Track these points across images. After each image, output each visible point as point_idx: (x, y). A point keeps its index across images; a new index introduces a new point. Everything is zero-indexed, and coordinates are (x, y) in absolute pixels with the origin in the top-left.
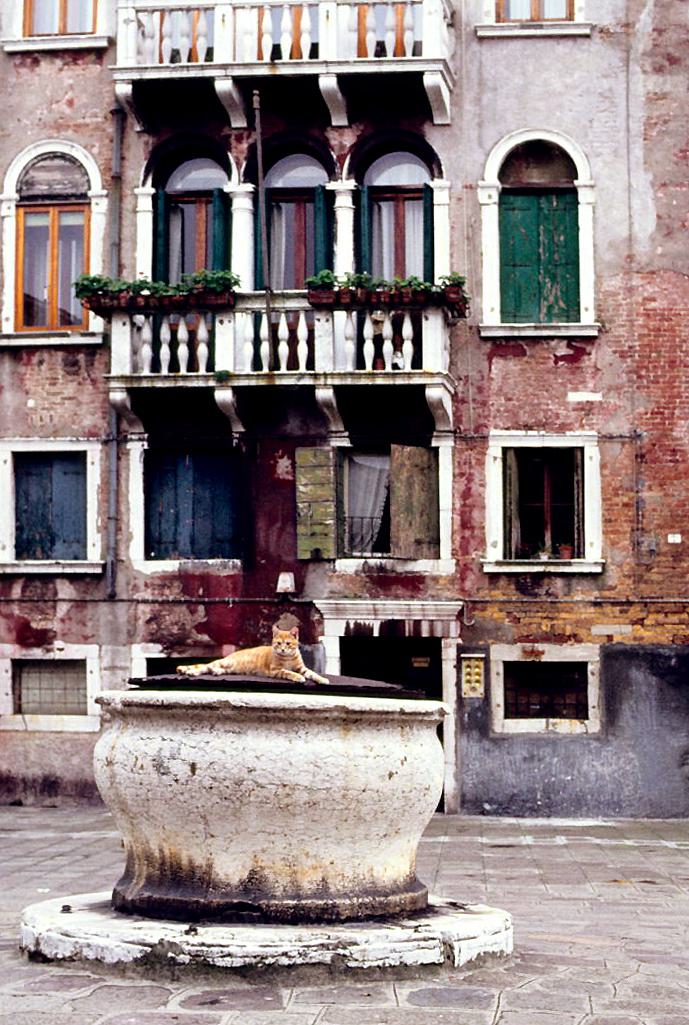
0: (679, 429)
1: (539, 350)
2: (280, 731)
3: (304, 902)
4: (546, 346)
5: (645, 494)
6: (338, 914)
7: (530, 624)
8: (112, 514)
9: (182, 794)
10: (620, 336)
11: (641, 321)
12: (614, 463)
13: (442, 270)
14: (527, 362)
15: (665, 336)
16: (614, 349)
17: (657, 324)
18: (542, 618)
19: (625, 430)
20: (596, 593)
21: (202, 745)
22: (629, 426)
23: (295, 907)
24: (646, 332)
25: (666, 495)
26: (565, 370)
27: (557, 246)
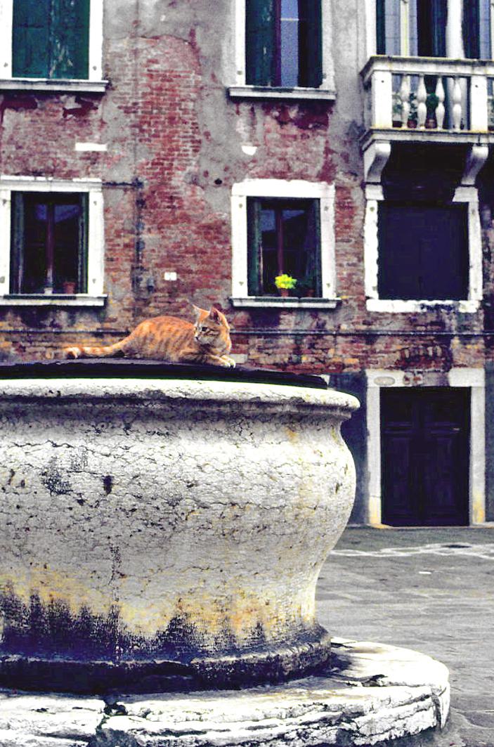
0: (176, 179)
1: (48, 104)
2: (219, 432)
3: (244, 657)
4: (56, 100)
5: (145, 237)
6: (282, 669)
7: (36, 352)
9: (88, 519)
10: (125, 93)
11: (145, 80)
12: (117, 208)
14: (37, 114)
15: (166, 94)
16: (119, 104)
17: (159, 83)
18: (46, 347)
19: (128, 178)
20: (98, 325)
21: (120, 452)
22: (133, 175)
23: (237, 665)
24: (149, 90)
25: (164, 237)
26: (74, 122)
27: (68, 11)
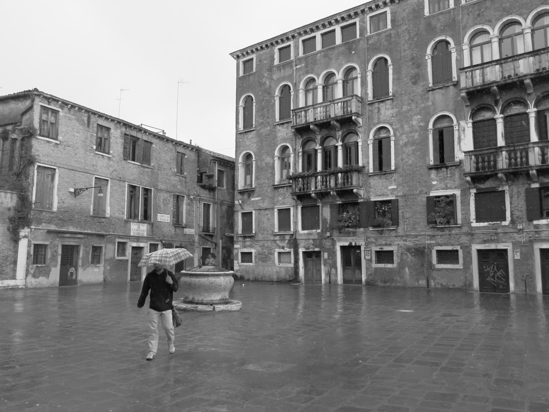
8: (295, 221)
13: (360, 164)
23: (25, 94)
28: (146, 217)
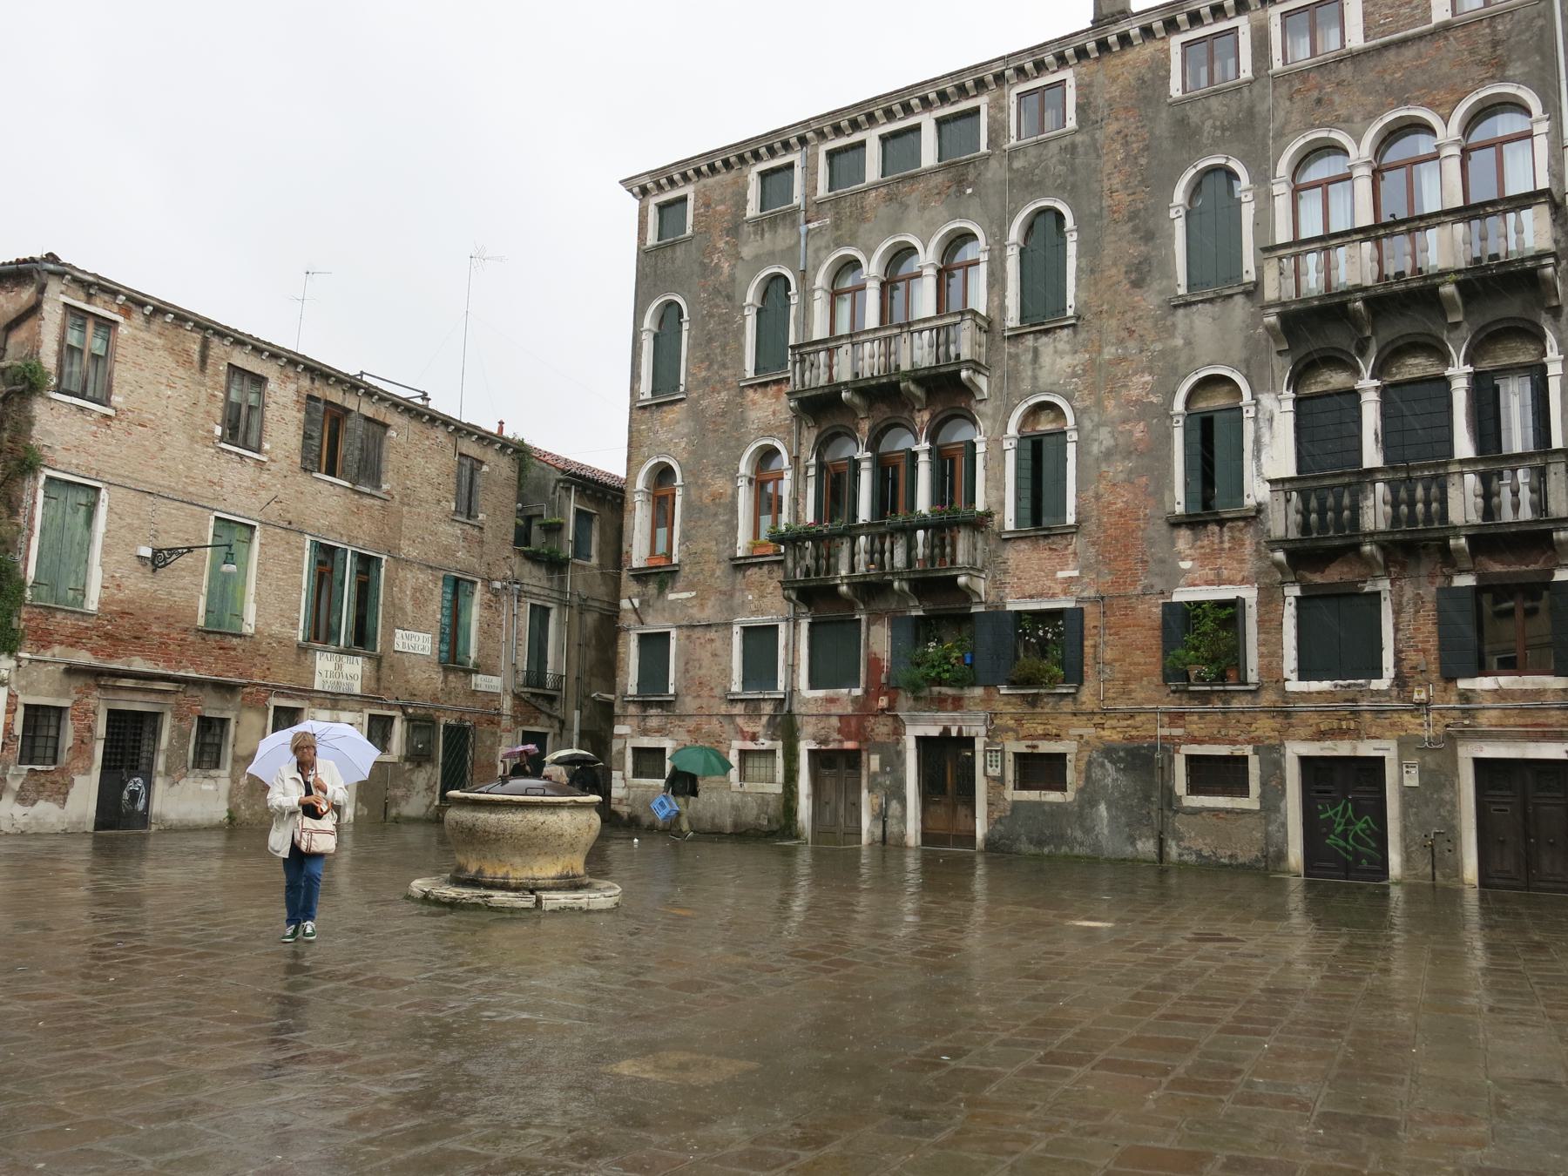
13: (980, 506)
28: (362, 638)
